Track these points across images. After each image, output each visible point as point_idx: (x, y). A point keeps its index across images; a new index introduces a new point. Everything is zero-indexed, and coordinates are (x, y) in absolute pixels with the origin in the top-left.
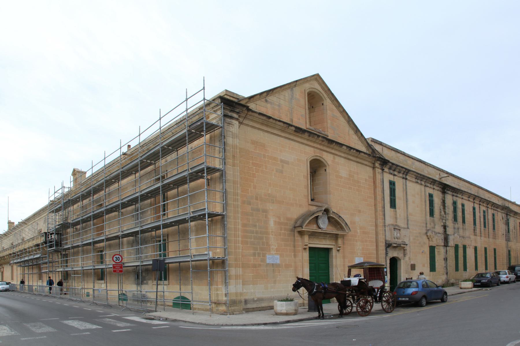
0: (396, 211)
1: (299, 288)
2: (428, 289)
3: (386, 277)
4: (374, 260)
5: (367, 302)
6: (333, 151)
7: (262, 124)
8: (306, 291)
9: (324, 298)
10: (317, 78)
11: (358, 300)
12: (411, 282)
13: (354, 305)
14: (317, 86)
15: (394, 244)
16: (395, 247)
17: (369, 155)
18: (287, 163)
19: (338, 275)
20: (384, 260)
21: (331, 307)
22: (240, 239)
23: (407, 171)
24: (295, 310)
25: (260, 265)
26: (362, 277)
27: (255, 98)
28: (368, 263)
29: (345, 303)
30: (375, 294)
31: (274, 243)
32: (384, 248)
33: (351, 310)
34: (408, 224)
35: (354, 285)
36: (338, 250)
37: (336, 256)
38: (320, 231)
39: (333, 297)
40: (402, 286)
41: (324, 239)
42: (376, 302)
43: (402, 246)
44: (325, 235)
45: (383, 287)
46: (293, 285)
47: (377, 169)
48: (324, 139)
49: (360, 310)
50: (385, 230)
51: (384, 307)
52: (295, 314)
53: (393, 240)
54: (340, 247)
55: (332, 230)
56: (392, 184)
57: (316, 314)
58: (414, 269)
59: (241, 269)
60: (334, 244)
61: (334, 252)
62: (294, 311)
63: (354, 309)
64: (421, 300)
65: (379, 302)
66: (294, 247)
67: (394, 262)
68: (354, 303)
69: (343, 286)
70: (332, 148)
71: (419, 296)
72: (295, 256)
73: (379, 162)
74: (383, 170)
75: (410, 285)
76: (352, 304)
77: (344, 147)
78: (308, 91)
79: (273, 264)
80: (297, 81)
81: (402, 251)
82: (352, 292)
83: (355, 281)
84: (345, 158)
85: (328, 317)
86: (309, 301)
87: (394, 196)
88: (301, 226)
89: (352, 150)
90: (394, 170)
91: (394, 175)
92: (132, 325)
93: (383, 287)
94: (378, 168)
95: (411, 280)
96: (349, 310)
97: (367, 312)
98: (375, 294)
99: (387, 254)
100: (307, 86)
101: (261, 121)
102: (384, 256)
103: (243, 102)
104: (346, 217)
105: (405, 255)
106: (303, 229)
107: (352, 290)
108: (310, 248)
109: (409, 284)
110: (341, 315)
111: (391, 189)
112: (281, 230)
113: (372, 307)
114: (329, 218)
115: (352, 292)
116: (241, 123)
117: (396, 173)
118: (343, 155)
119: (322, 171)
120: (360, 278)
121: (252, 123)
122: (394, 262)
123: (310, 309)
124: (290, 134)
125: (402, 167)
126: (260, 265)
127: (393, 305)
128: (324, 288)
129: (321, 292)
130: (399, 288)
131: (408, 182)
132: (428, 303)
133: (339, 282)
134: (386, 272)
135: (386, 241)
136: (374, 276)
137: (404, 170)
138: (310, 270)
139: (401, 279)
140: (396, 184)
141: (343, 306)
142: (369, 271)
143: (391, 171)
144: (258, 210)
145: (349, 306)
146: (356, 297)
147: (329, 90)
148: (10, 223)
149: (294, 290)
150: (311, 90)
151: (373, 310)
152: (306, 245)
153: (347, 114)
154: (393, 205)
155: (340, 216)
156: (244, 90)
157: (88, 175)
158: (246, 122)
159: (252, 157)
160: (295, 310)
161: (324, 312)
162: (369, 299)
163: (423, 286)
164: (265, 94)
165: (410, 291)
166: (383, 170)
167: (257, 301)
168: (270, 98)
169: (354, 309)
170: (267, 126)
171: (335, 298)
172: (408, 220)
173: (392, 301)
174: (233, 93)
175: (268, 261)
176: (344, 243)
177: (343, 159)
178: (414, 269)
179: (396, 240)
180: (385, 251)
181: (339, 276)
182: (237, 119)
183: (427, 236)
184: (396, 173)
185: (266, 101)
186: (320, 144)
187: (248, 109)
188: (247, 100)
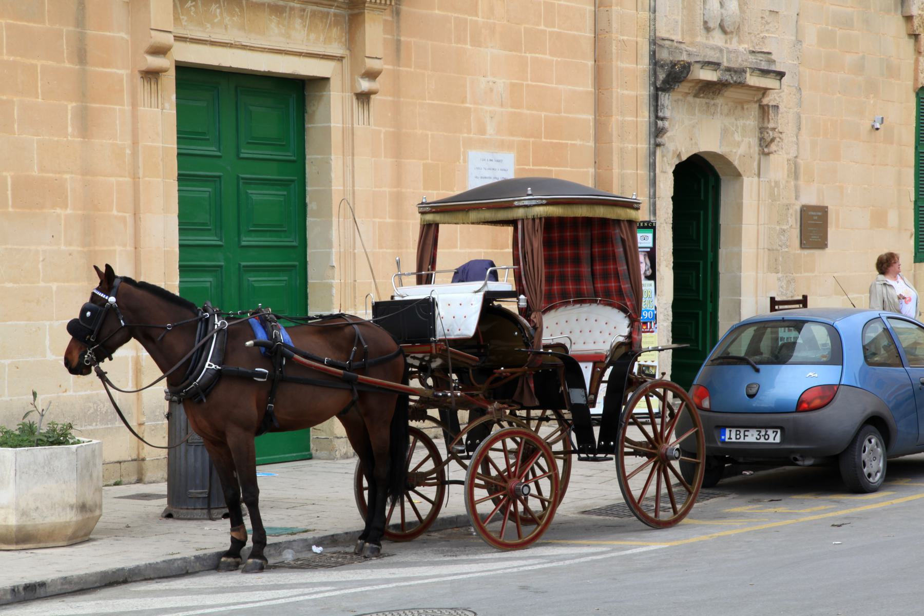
1: (106, 351)
2: (897, 372)
3: (647, 286)
4: (579, 174)
5: (531, 449)
8: (152, 370)
9: (267, 423)
11: (479, 433)
12: (798, 325)
13: (454, 471)
15: (707, 64)
16: (708, 89)
19: (357, 264)
20: (644, 172)
21: (313, 486)
24: (83, 508)
26: (506, 283)
28: (537, 184)
29: (400, 454)
30: (577, 396)
32: (643, 92)
33: (437, 504)
35: (455, 334)
36: (364, 97)
37: (350, 134)
39: (321, 417)
40: (741, 348)
42: (589, 450)
43: (753, 80)
45: (628, 350)
46: (73, 327)
49: (486, 507)
51: (636, 485)
52: (80, 536)
53: (701, 38)
54: (372, 75)
57: (216, 535)
58: (822, 244)
60: (336, 49)
61: (336, 111)
62: (71, 517)
63: (455, 502)
64: (855, 442)
65: (607, 449)
66: (81, 55)
67: (699, 185)
68: (453, 455)
69: (387, 340)
71: (841, 418)
72: (86, 123)
75: (791, 346)
76: (440, 465)
81: (751, 121)
82: (442, 382)
83: (458, 311)
85: (288, 556)
86: (171, 447)
93: (628, 350)
95: (797, 313)
96: (425, 509)
97: (528, 518)
98: (577, 396)
99: (657, 132)
102: (643, 146)
105: (765, 144)
107: (444, 369)
109: (785, 334)
110: (377, 536)
113: (560, 487)
115: (442, 382)
120: (493, 286)
122: (699, 185)
123: (181, 503)
127: (687, 478)
128: (272, 352)
129: (247, 378)
130: (728, 360)
132: (899, 471)
133: (367, 315)
134: (652, 255)
136: (578, 278)
138: (184, 229)
139: (738, 304)
141: (383, 475)
142: (548, 244)
145: (421, 479)
146: (463, 415)
149: (77, 366)
151: (566, 509)
152: (159, 51)
160: (83, 508)
161: (268, 519)
162: (547, 430)
163: (869, 352)
165: (790, 383)
169: (455, 502)
171: (336, 427)
173: (682, 450)
176: (397, 49)
178: (822, 244)
179: (718, 39)
180: (645, 116)
181: (363, 276)
183: (909, 18)
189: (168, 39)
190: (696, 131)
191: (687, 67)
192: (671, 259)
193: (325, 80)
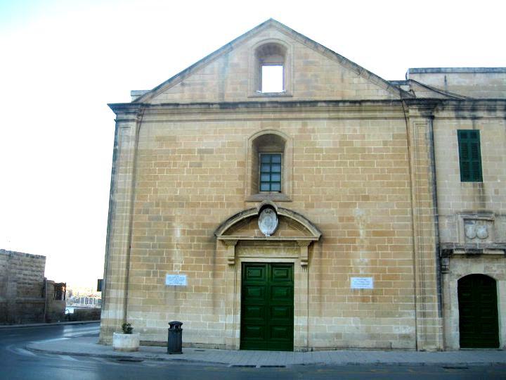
6: (303, 115)
7: (173, 114)
18: (210, 152)
25: (155, 287)
31: (178, 258)
32: (434, 258)
41: (276, 249)
44: (274, 243)
58: (172, 324)
60: (296, 256)
66: (214, 262)
77: (268, 105)
79: (175, 286)
91: (474, 118)
99: (442, 271)
101: (199, 111)
112: (192, 240)
124: (216, 113)
126: (155, 287)
143: (466, 114)
144: (158, 218)
155: (295, 213)
158: (146, 118)
159: (156, 157)
167: (147, 332)
175: (168, 282)
177: (325, 122)
186: (274, 112)
188: (151, 95)
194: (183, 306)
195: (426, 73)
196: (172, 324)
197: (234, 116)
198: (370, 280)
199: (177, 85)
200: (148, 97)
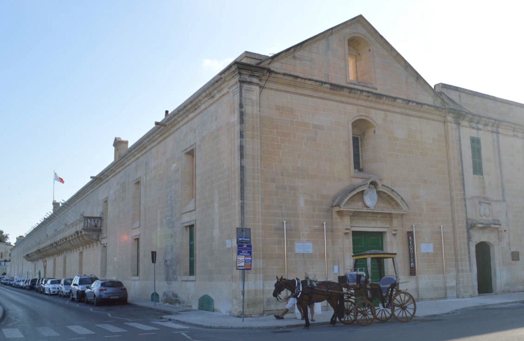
0: (483, 179)
6: (385, 107)
7: (289, 85)
10: (360, 20)
14: (361, 31)
17: (436, 108)
20: (466, 246)
22: (260, 224)
23: (497, 122)
27: (280, 56)
32: (465, 230)
34: (503, 196)
36: (394, 235)
38: (365, 210)
41: (374, 220)
44: (373, 215)
47: (449, 124)
48: (370, 94)
50: (465, 205)
55: (385, 208)
56: (475, 143)
58: (518, 260)
59: (261, 261)
60: (388, 226)
70: (383, 104)
73: (451, 115)
74: (458, 124)
77: (364, 93)
78: (349, 37)
79: (303, 254)
80: (332, 28)
84: (402, 114)
87: (480, 157)
88: (338, 205)
89: (411, 103)
90: (478, 123)
91: (478, 129)
92: (155, 329)
94: (451, 122)
99: (469, 238)
100: (348, 32)
103: (264, 65)
104: (404, 192)
105: (500, 239)
106: (341, 209)
108: (354, 233)
111: (473, 148)
114: (378, 192)
116: (262, 87)
117: (480, 126)
118: (398, 110)
119: (370, 133)
121: (276, 85)
124: (325, 92)
125: (488, 118)
131: (501, 137)
135: (467, 219)
137: (493, 121)
140: (482, 141)
143: (474, 125)
147: (376, 32)
148: (55, 204)
150: (353, 35)
152: (347, 229)
153: (404, 59)
154: (478, 169)
155: (393, 190)
156: (268, 49)
157: (130, 145)
158: (268, 85)
159: (277, 125)
164: (292, 50)
166: (458, 124)
168: (298, 54)
170: (295, 86)
172: (503, 190)
174: (255, 54)
177: (399, 115)
179: (484, 218)
180: (466, 235)
182: (258, 84)
184: (480, 126)
185: (294, 58)
186: (366, 100)
187: (270, 71)
188: (269, 61)
189: (349, 227)
190: (478, 237)
191: (475, 224)
192: (476, 264)
193: (386, 232)
194: (310, 273)
195: (450, 89)
196: (518, 260)
197: (338, 98)
198: (432, 245)
199: (289, 57)
200: (267, 62)
